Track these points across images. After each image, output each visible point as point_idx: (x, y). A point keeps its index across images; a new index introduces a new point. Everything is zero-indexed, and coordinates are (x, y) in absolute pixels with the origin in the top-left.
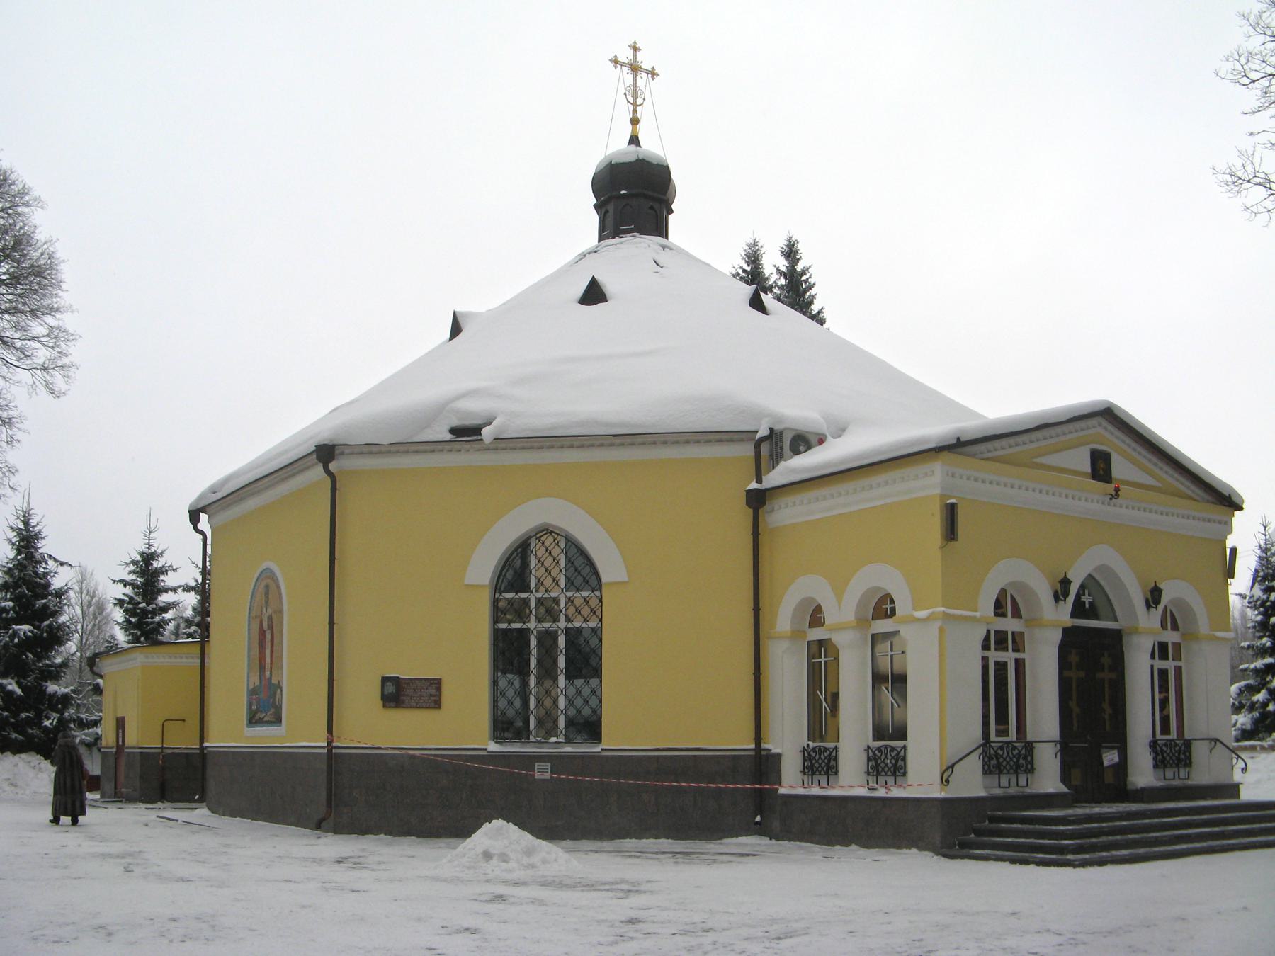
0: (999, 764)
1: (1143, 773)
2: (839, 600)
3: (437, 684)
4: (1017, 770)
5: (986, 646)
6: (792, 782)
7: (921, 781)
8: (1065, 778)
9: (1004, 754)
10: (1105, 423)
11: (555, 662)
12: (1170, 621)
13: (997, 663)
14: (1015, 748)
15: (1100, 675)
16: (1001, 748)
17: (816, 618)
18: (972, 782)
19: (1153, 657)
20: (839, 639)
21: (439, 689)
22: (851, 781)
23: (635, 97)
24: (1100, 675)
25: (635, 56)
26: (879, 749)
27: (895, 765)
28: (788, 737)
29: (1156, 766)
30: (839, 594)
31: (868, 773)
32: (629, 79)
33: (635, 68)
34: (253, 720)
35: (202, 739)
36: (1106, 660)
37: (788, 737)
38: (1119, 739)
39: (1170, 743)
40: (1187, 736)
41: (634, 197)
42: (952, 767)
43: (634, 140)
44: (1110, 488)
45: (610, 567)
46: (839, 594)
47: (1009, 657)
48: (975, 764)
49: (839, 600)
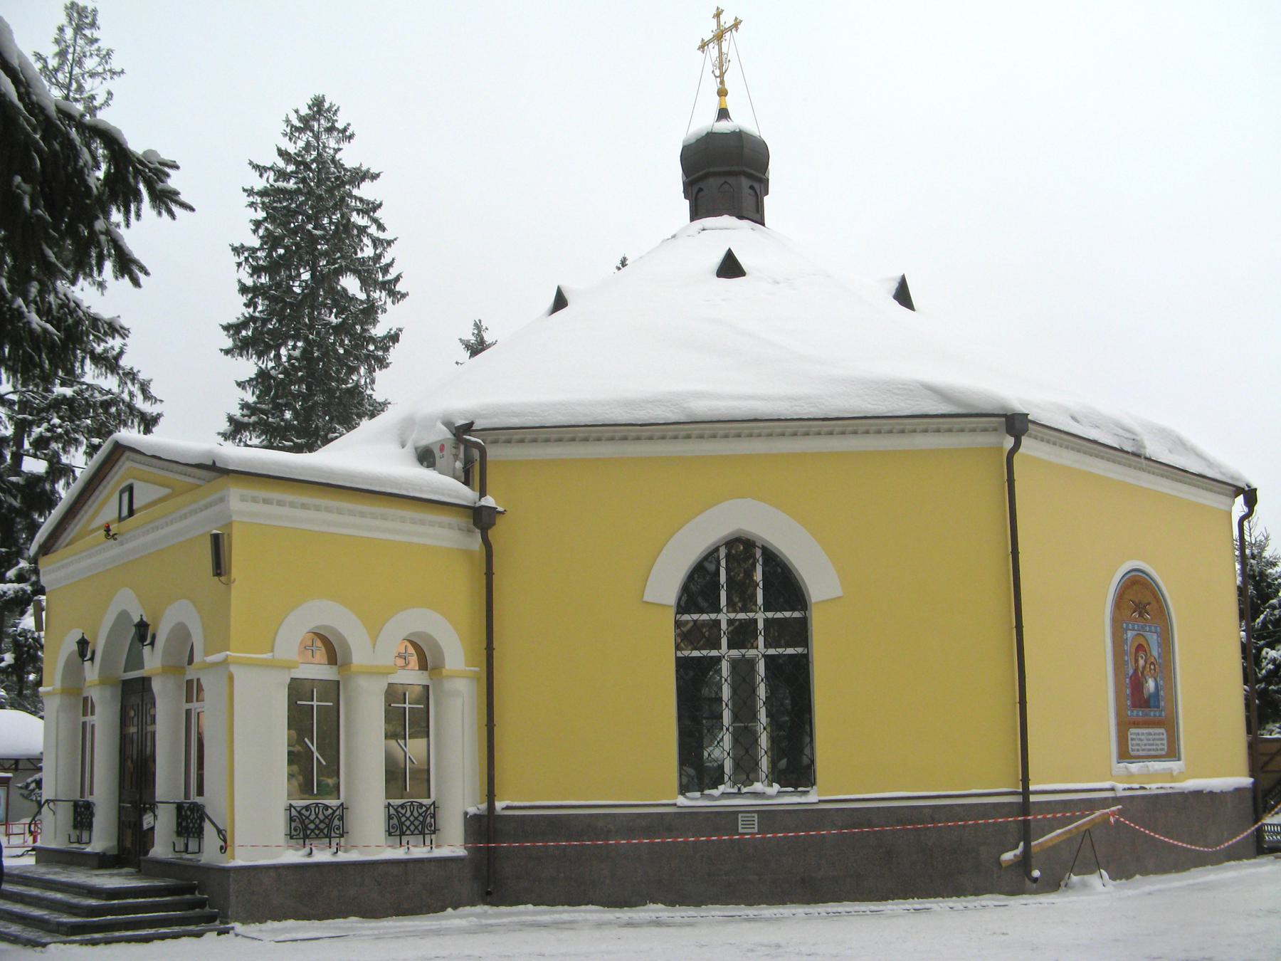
2: (374, 639)
11: (735, 691)
22: (370, 841)
35: (491, 797)
41: (725, 174)
43: (723, 114)
45: (820, 580)
49: (374, 639)
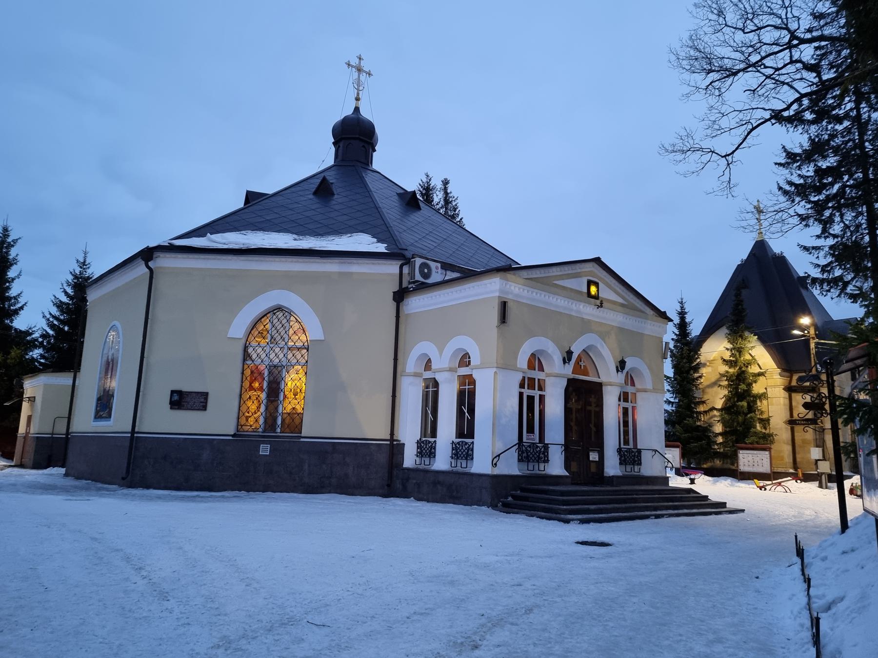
0: (528, 456)
1: (612, 467)
2: (441, 355)
3: (205, 395)
4: (538, 460)
5: (522, 386)
6: (410, 459)
7: (481, 464)
8: (567, 467)
9: (531, 452)
10: (596, 266)
12: (630, 380)
13: (528, 396)
14: (537, 447)
15: (589, 408)
16: (529, 446)
17: (428, 366)
18: (511, 467)
19: (620, 400)
20: (439, 377)
21: (206, 399)
22: (442, 462)
23: (359, 85)
24: (589, 408)
25: (360, 63)
26: (458, 443)
27: (467, 453)
28: (409, 433)
29: (621, 464)
30: (441, 352)
31: (452, 457)
32: (356, 75)
33: (359, 70)
34: (98, 417)
36: (593, 400)
37: (409, 433)
38: (599, 446)
39: (629, 451)
40: (639, 447)
42: (499, 456)
44: (598, 302)
46: (441, 352)
47: (536, 393)
48: (514, 454)
